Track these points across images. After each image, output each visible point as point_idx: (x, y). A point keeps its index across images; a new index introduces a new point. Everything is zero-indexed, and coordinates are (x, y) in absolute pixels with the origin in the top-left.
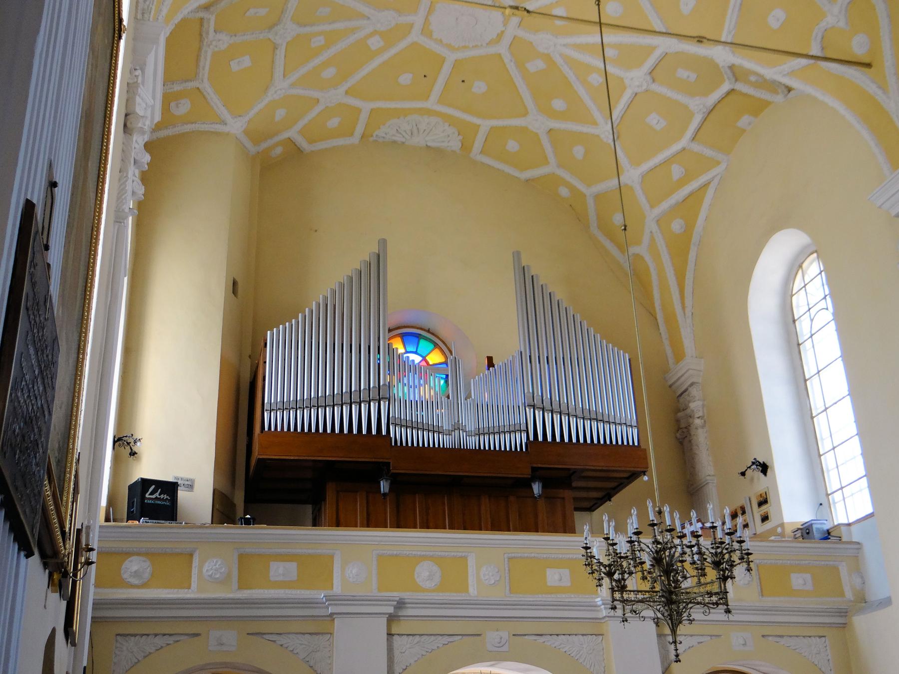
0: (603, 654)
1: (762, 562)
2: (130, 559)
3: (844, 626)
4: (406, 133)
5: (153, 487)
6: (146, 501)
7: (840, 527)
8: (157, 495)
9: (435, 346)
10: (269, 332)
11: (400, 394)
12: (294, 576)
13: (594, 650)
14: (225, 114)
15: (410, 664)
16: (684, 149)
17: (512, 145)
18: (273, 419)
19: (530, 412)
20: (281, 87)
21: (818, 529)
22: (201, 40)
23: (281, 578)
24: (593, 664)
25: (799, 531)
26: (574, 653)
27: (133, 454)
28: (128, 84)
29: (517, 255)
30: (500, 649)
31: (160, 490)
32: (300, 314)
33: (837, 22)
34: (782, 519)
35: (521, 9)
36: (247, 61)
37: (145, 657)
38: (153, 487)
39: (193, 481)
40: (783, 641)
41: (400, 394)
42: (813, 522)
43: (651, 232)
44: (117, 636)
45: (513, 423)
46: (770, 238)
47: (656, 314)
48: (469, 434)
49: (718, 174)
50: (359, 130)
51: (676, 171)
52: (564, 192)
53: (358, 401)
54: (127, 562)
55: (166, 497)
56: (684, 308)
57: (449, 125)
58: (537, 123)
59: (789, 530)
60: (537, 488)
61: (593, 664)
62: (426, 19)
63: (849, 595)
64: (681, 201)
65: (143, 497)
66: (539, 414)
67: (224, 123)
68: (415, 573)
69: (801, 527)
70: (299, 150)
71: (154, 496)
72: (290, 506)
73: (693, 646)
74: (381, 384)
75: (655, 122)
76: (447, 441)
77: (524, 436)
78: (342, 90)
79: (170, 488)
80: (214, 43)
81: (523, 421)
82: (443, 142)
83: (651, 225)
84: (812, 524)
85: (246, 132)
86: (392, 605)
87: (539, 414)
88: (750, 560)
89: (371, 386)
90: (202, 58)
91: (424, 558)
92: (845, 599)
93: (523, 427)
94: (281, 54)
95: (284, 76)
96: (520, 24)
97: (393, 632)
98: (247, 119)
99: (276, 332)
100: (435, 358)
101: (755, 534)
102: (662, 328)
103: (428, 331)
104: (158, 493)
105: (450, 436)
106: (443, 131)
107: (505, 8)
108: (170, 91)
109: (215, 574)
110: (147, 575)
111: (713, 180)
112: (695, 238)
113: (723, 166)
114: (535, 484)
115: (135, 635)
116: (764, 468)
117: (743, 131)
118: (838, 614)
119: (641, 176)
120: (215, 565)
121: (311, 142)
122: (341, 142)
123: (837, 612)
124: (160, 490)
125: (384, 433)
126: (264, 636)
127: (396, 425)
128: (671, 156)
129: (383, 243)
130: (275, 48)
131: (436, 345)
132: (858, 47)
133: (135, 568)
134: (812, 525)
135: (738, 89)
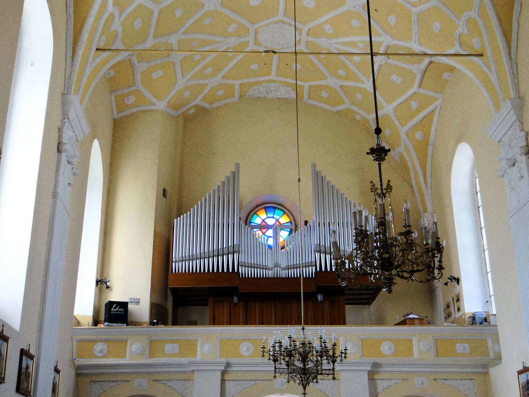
0: (339, 390)
1: (438, 338)
2: (98, 344)
3: (487, 373)
4: (264, 92)
5: (115, 305)
6: (111, 312)
7: (489, 317)
8: (117, 309)
9: (284, 213)
10: (175, 220)
11: (263, 242)
12: (177, 350)
13: (334, 387)
14: (154, 100)
15: (234, 395)
16: (415, 93)
17: (324, 94)
18: (177, 266)
19: (317, 255)
20: (181, 83)
21: (479, 317)
22: (133, 67)
23: (171, 352)
24: (333, 395)
25: (471, 318)
26: (323, 389)
27: (108, 287)
28: (59, 128)
29: (314, 165)
30: (282, 388)
31: (119, 306)
32: (192, 209)
33: (463, 31)
34: (465, 311)
35: (270, 52)
36: (161, 73)
37: (103, 392)
38: (115, 305)
39: (139, 300)
40: (447, 382)
41: (263, 242)
42: (476, 313)
43: (404, 140)
44: (91, 382)
45: (308, 262)
46: (457, 148)
47: (413, 186)
48: (283, 269)
49: (439, 105)
50: (237, 94)
51: (414, 105)
52: (358, 118)
53: (222, 254)
54: (96, 346)
55: (122, 310)
56: (426, 183)
57: (287, 86)
58: (333, 82)
59: (467, 316)
60: (320, 297)
61: (333, 395)
62: (255, 37)
63: (492, 355)
64: (419, 122)
65: (110, 310)
66: (323, 256)
67: (155, 105)
68: (240, 348)
69: (472, 316)
70: (205, 109)
71: (115, 310)
72: (201, 307)
73: (392, 385)
74: (235, 244)
75: (395, 79)
76: (270, 274)
77: (314, 268)
78: (219, 77)
79: (124, 305)
80: (139, 68)
81: (314, 260)
82: (286, 95)
83: (403, 137)
84: (475, 315)
85: (168, 106)
86: (223, 366)
87: (323, 256)
88: (346, 353)
89: (229, 246)
90: (136, 76)
91: (244, 340)
92: (489, 358)
93: (314, 264)
94: (178, 66)
95: (183, 77)
96: (308, 34)
97: (225, 379)
98: (167, 100)
99: (182, 218)
100: (284, 220)
101: (455, 318)
102: (417, 194)
103: (280, 205)
104: (118, 308)
105: (272, 271)
106: (285, 90)
107: (262, 52)
108: (123, 93)
109: (138, 351)
110: (105, 352)
111: (436, 108)
112: (430, 142)
113: (440, 100)
114: (318, 295)
115: (99, 381)
116: (458, 280)
117: (447, 81)
118: (482, 367)
119: (393, 109)
120: (138, 346)
121: (211, 103)
122: (228, 101)
123: (481, 366)
124: (119, 306)
125: (236, 271)
126: (161, 381)
127: (242, 266)
128: (409, 97)
129: (238, 166)
130: (174, 64)
131: (285, 213)
132: (476, 44)
133: (99, 349)
134: (475, 315)
135: (434, 61)
